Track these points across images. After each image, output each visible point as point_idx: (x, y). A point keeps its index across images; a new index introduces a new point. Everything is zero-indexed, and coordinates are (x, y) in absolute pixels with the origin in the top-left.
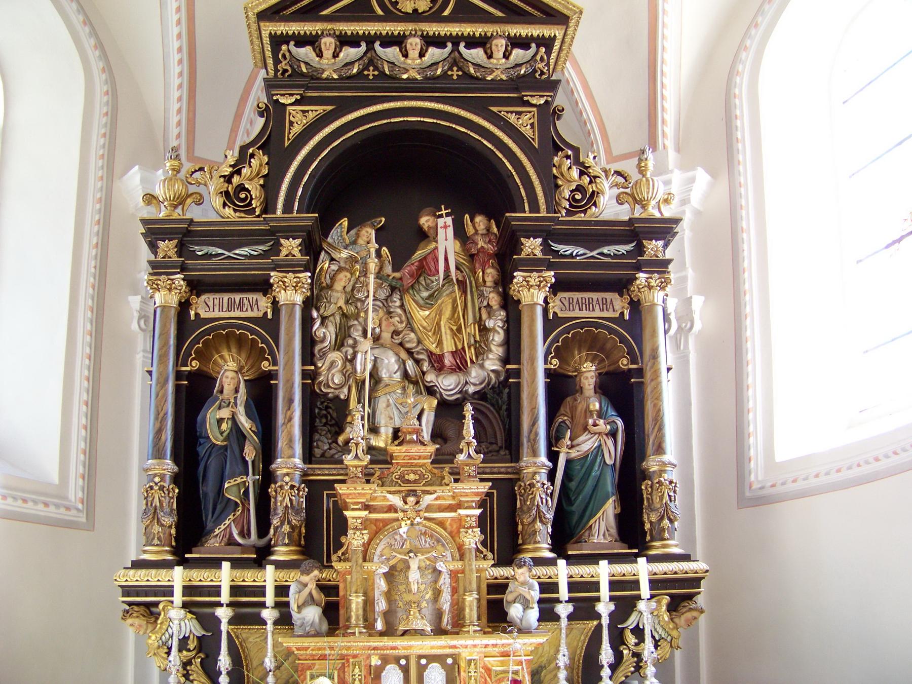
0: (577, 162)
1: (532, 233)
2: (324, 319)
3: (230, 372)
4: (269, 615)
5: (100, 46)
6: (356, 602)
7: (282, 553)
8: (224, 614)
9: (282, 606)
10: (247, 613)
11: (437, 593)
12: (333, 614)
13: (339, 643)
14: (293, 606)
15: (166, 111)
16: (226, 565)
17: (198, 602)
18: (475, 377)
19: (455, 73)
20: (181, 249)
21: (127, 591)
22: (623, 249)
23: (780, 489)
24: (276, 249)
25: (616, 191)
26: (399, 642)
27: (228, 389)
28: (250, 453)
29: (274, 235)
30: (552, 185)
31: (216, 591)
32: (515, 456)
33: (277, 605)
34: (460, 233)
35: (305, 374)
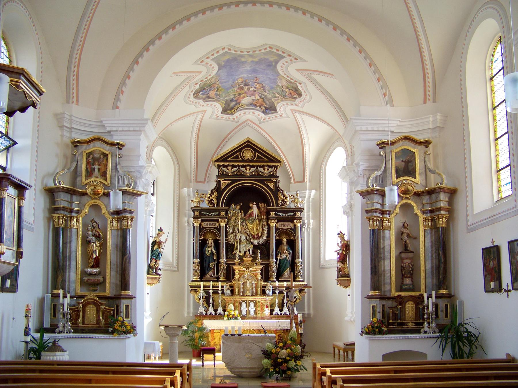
0: (283, 194)
1: (273, 211)
2: (229, 227)
3: (210, 241)
4: (220, 292)
5: (177, 158)
6: (237, 289)
7: (222, 279)
8: (211, 291)
9: (222, 290)
10: (216, 292)
11: (252, 288)
12: (232, 292)
13: (234, 298)
14: (225, 290)
15: (191, 171)
16: (211, 282)
17: (206, 289)
18: (261, 241)
19: (257, 174)
20: (200, 214)
21: (191, 287)
22: (292, 214)
23: (327, 266)
24: (219, 214)
25: (291, 200)
26: (245, 298)
27: (210, 243)
28: (215, 258)
29: (220, 211)
30: (277, 199)
31: (209, 287)
32: (269, 259)
33: (222, 290)
34: (258, 207)
35: (226, 240)
